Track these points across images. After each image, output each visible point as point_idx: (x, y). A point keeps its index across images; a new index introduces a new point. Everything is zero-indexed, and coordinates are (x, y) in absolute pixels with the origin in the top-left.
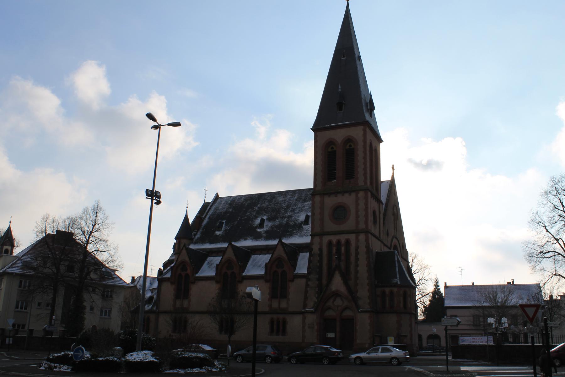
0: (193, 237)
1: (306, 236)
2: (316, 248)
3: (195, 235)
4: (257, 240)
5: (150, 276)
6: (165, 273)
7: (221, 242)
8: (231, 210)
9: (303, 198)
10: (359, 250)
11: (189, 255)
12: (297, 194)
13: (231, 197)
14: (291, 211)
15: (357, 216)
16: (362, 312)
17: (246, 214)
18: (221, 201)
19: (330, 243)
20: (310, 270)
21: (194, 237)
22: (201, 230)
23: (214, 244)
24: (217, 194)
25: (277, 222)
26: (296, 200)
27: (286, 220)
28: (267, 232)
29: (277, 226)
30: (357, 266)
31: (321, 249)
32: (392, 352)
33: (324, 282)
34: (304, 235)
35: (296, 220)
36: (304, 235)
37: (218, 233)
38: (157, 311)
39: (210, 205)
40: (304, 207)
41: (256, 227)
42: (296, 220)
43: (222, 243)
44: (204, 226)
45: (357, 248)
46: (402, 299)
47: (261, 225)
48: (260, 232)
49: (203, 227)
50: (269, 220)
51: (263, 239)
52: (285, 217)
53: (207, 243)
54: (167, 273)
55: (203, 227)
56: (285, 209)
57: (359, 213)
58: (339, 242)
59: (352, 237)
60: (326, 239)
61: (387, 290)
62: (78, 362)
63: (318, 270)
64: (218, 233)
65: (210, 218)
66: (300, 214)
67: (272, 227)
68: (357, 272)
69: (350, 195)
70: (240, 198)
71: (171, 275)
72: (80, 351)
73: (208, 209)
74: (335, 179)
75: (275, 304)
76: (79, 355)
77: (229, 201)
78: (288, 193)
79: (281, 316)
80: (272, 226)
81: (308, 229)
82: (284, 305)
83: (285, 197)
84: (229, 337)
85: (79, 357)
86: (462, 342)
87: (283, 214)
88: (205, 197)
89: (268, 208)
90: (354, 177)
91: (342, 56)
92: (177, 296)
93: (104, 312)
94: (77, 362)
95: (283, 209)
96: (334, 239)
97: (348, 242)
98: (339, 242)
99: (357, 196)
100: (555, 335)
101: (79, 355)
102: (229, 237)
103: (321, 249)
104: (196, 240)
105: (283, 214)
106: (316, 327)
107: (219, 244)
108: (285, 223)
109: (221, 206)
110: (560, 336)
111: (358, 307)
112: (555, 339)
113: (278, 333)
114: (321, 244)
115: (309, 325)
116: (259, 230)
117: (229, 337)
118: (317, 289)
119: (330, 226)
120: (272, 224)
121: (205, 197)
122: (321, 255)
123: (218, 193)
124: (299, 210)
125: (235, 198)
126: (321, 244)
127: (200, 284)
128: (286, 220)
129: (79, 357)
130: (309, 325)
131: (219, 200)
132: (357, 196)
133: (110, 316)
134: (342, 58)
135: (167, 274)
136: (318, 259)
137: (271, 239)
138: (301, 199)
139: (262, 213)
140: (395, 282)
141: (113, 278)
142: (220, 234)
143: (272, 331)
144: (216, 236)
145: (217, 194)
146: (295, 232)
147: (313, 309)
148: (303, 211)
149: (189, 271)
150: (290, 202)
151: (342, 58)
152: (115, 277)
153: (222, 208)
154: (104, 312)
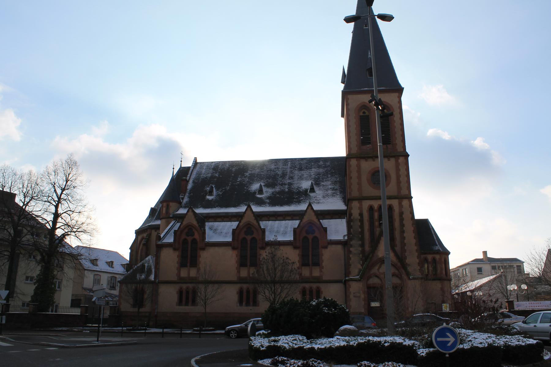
0: (182, 201)
1: (316, 203)
2: (355, 213)
3: (183, 199)
4: (260, 206)
5: (89, 246)
6: (163, 238)
7: (217, 206)
8: (217, 175)
9: (298, 166)
10: (404, 216)
11: (197, 218)
12: (289, 163)
13: (212, 162)
14: (289, 178)
15: (359, 177)
16: (414, 279)
17: (237, 179)
18: (201, 165)
19: (371, 208)
20: (351, 235)
21: (183, 201)
22: (187, 194)
23: (210, 209)
24: (196, 159)
25: (278, 189)
26: (291, 168)
27: (287, 186)
28: (269, 198)
29: (279, 193)
30: (402, 232)
31: (361, 215)
32: (512, 317)
33: (367, 248)
34: (314, 202)
35: (299, 188)
36: (314, 202)
37: (209, 198)
38: (157, 281)
39: (191, 169)
40: (303, 175)
41: (255, 193)
42: (299, 188)
43: (219, 208)
44: (190, 191)
45: (401, 214)
46: (443, 265)
47: (261, 191)
48: (261, 198)
49: (188, 191)
50: (267, 186)
51: (267, 205)
52: (285, 184)
53: (200, 207)
54: (166, 236)
55: (188, 191)
56: (281, 176)
57: (401, 179)
58: (380, 207)
59: (395, 203)
60: (366, 204)
61: (430, 257)
62: (449, 354)
63: (360, 236)
64: (209, 198)
65: (194, 182)
66: (301, 182)
67: (273, 193)
68: (403, 238)
69: (389, 160)
70: (223, 163)
71: (174, 240)
72: (448, 334)
73: (190, 173)
74: (369, 143)
75: (184, 273)
76: (449, 342)
77: (211, 166)
78: (278, 161)
79: (314, 286)
80: (273, 192)
81: (316, 196)
82: (316, 273)
83: (277, 165)
84: (139, 310)
85: (449, 344)
86: (518, 307)
87: (281, 181)
88: (181, 161)
89: (261, 175)
90: (390, 143)
91: (364, 26)
92: (183, 264)
93: (97, 281)
94: (447, 356)
95: (279, 176)
96: (376, 204)
97: (390, 208)
98: (371, 208)
99: (397, 161)
100: (61, 306)
101: (449, 342)
102: (191, 205)
103: (361, 215)
104: (185, 204)
105: (281, 181)
106: (363, 296)
107: (215, 209)
108: (287, 190)
109: (203, 171)
110: (65, 307)
111: (408, 274)
112: (61, 309)
113: (248, 304)
114: (361, 208)
115: (354, 293)
116: (259, 196)
117: (139, 310)
118: (361, 255)
119: (369, 190)
120: (273, 190)
121: (181, 161)
122: (361, 221)
123: (196, 158)
124: (299, 178)
125: (217, 164)
126: (361, 208)
127: (212, 250)
128: (287, 186)
129: (449, 344)
130: (354, 293)
131: (198, 165)
132: (397, 161)
133: (59, 288)
134: (365, 28)
135: (164, 240)
136: (359, 224)
137: (278, 205)
138: (296, 167)
139: (256, 179)
140: (437, 249)
141: (64, 246)
142: (213, 199)
143: (241, 302)
144: (208, 200)
145: (196, 159)
146: (303, 199)
147: (358, 277)
148: (303, 179)
149: (197, 236)
150: (285, 170)
151: (365, 28)
152: (65, 245)
153: (205, 173)
154: (97, 281)
